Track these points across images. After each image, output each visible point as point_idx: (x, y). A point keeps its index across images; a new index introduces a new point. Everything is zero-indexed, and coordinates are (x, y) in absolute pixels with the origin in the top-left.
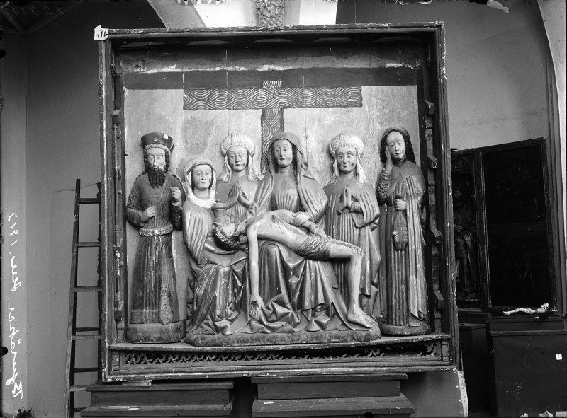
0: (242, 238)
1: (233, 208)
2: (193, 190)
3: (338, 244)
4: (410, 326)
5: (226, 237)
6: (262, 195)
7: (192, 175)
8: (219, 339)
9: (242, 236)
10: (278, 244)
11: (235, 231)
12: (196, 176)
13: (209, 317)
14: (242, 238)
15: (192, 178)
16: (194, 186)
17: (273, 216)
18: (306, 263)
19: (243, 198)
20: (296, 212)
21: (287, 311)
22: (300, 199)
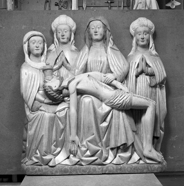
0: (65, 91)
1: (58, 55)
2: (29, 56)
3: (138, 97)
4: (142, 72)
5: (53, 90)
6: (80, 61)
7: (29, 43)
8: (46, 169)
9: (65, 90)
10: (91, 96)
11: (60, 86)
12: (31, 44)
13: (38, 151)
14: (65, 91)
15: (29, 46)
16: (29, 53)
17: (89, 75)
18: (113, 112)
19: (66, 62)
20: (106, 73)
21: (97, 148)
22: (140, 139)
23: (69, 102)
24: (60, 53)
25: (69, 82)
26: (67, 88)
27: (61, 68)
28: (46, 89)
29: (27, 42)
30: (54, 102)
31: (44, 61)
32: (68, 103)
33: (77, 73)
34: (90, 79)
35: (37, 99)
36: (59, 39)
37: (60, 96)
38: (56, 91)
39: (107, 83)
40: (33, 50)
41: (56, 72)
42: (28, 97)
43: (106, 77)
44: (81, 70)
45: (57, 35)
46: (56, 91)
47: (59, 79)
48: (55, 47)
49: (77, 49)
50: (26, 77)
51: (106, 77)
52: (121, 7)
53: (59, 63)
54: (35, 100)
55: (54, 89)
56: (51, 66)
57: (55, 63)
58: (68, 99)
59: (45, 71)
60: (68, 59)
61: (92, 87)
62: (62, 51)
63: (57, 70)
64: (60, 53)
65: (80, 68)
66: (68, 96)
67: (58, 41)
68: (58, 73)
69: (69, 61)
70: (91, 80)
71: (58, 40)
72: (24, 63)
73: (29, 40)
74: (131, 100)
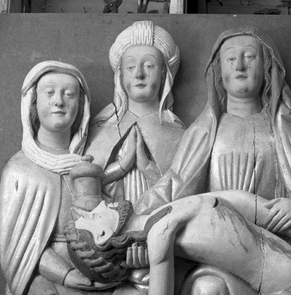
2: (35, 136)
7: (35, 95)
14: (133, 252)
15: (34, 102)
16: (36, 124)
23: (147, 287)
24: (129, 130)
25: (150, 224)
26: (143, 243)
27: (129, 175)
28: (72, 241)
29: (31, 90)
30: (98, 285)
31: (81, 151)
32: (144, 290)
33: (177, 193)
34: (222, 216)
35: (44, 272)
36: (129, 87)
37: (116, 268)
38: (104, 251)
39: (275, 229)
40: (46, 114)
41: (169, 75)
42: (14, 262)
43: (273, 210)
44: (188, 187)
45: (122, 76)
46: (111, 258)
47: (116, 209)
48: (116, 112)
49: (179, 120)
50: (16, 195)
51: (273, 210)
52: (79, 232)
53: (125, 155)
54: (36, 272)
55: (99, 241)
56: (98, 167)
57: (113, 158)
58: (144, 276)
59: (77, 180)
60: (152, 148)
61: (230, 241)
62: (135, 124)
63: (117, 180)
64: (129, 130)
65: (184, 177)
66: (145, 267)
67: (126, 94)
68: (120, 189)
69: (153, 155)
70: (227, 218)
71: (125, 91)
72: (18, 154)
73: (35, 84)
74: (85, 194)
